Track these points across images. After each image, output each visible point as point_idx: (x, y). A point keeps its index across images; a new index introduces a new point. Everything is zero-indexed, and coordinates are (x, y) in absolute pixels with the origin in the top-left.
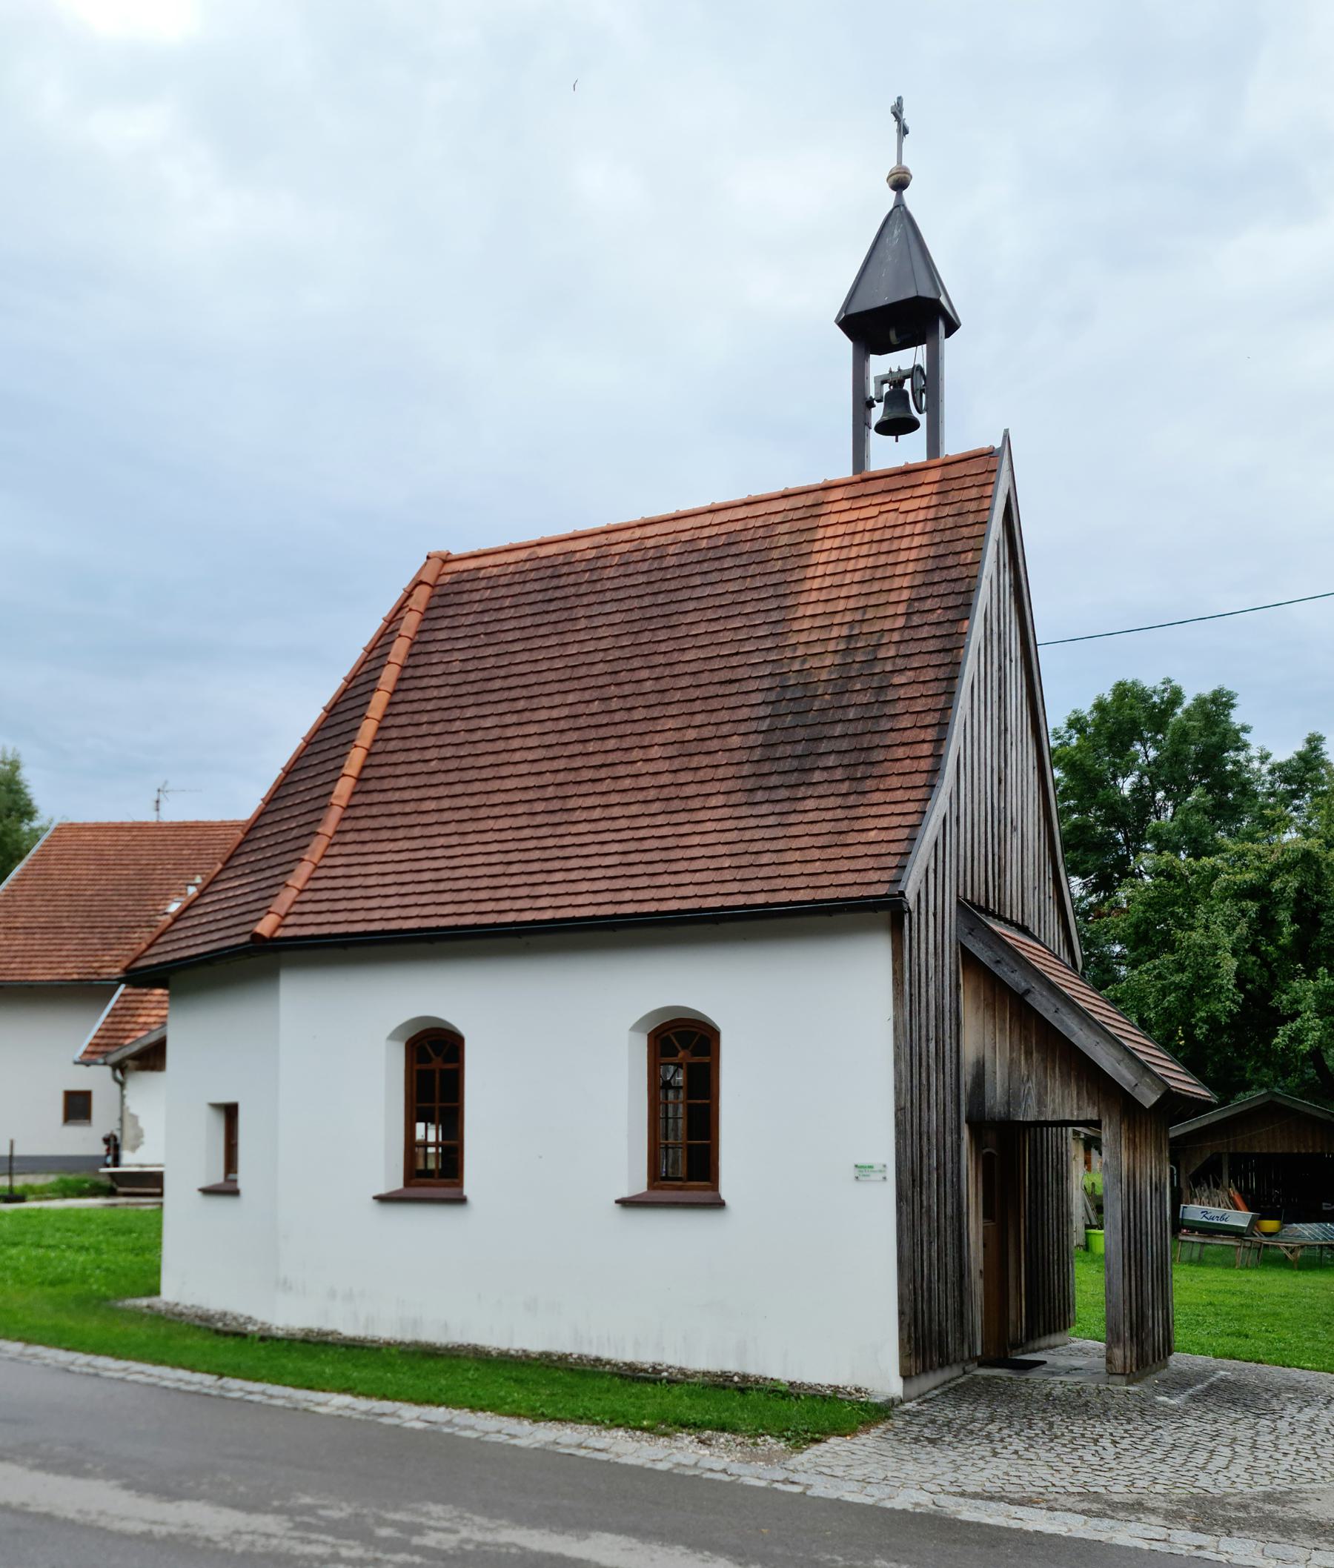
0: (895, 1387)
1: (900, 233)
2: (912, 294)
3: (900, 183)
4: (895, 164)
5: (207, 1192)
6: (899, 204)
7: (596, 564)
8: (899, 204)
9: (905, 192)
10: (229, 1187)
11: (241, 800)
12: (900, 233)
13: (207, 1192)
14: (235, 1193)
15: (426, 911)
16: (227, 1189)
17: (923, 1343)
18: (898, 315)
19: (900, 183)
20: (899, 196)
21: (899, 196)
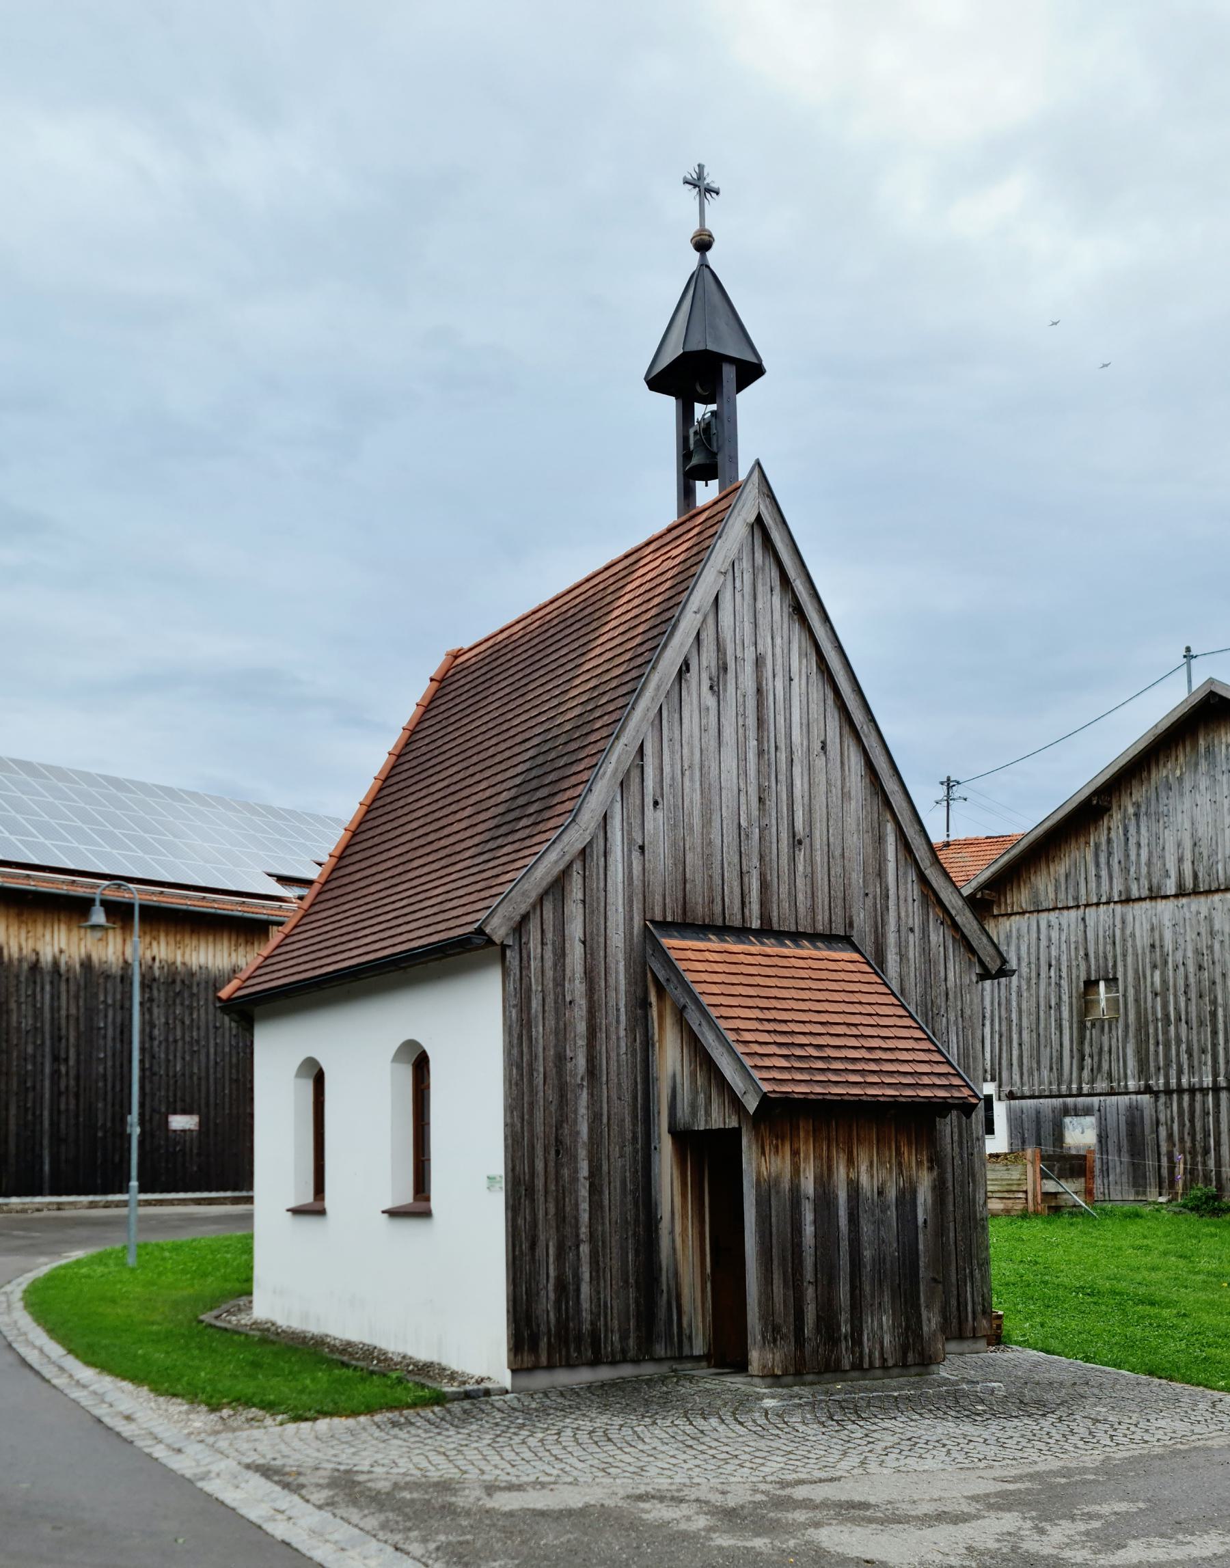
0: (503, 1377)
1: (705, 291)
2: (701, 347)
3: (703, 244)
4: (697, 227)
5: (393, 1213)
6: (703, 265)
7: (546, 625)
8: (703, 265)
9: (708, 254)
10: (317, 1207)
11: (310, 857)
12: (705, 291)
13: (393, 1213)
14: (321, 1212)
15: (802, 984)
16: (314, 1209)
17: (540, 1333)
18: (703, 372)
19: (703, 244)
20: (703, 257)
21: (703, 257)
